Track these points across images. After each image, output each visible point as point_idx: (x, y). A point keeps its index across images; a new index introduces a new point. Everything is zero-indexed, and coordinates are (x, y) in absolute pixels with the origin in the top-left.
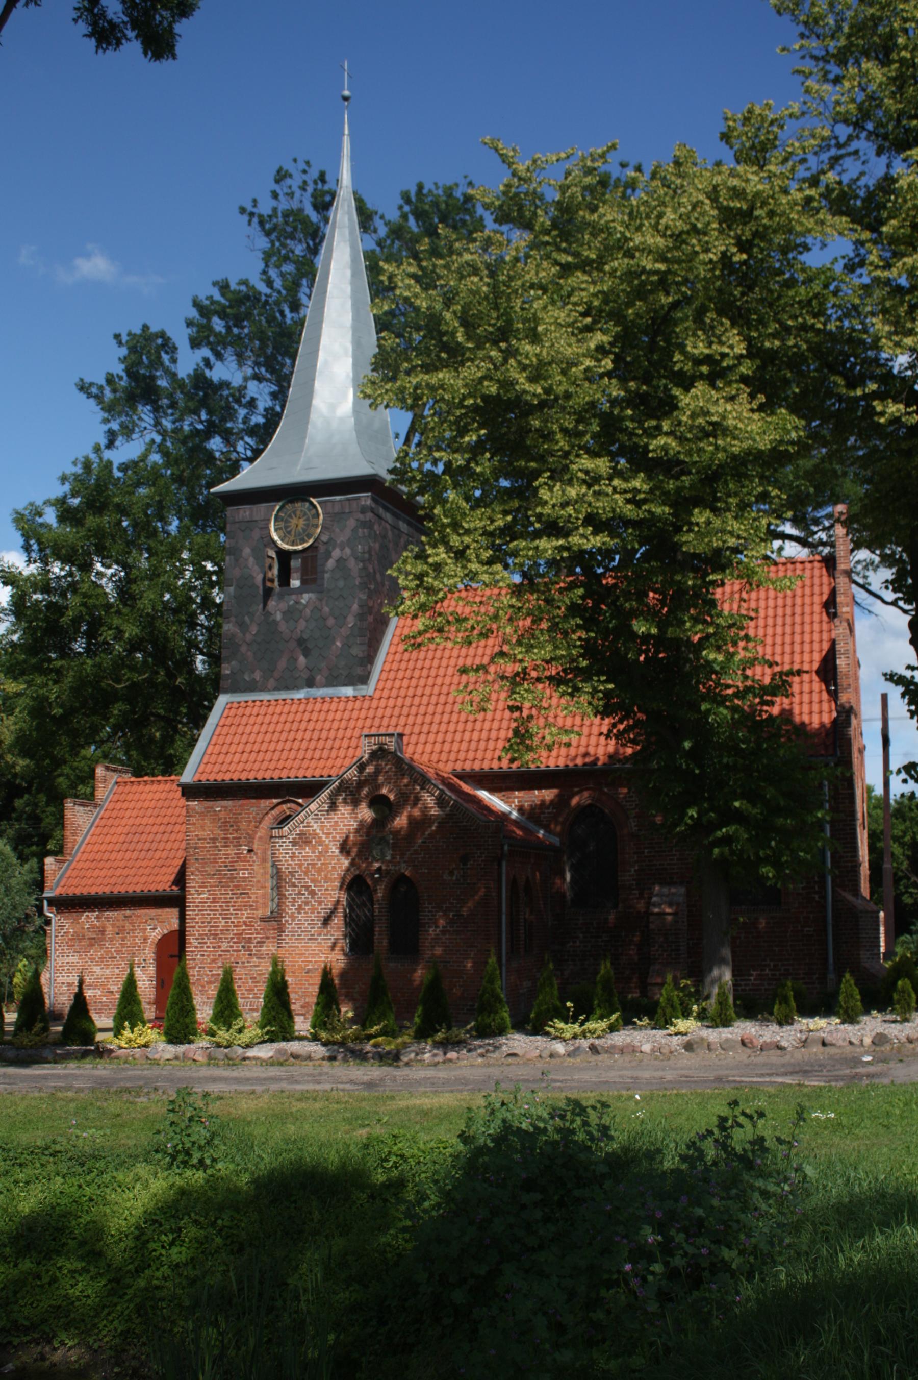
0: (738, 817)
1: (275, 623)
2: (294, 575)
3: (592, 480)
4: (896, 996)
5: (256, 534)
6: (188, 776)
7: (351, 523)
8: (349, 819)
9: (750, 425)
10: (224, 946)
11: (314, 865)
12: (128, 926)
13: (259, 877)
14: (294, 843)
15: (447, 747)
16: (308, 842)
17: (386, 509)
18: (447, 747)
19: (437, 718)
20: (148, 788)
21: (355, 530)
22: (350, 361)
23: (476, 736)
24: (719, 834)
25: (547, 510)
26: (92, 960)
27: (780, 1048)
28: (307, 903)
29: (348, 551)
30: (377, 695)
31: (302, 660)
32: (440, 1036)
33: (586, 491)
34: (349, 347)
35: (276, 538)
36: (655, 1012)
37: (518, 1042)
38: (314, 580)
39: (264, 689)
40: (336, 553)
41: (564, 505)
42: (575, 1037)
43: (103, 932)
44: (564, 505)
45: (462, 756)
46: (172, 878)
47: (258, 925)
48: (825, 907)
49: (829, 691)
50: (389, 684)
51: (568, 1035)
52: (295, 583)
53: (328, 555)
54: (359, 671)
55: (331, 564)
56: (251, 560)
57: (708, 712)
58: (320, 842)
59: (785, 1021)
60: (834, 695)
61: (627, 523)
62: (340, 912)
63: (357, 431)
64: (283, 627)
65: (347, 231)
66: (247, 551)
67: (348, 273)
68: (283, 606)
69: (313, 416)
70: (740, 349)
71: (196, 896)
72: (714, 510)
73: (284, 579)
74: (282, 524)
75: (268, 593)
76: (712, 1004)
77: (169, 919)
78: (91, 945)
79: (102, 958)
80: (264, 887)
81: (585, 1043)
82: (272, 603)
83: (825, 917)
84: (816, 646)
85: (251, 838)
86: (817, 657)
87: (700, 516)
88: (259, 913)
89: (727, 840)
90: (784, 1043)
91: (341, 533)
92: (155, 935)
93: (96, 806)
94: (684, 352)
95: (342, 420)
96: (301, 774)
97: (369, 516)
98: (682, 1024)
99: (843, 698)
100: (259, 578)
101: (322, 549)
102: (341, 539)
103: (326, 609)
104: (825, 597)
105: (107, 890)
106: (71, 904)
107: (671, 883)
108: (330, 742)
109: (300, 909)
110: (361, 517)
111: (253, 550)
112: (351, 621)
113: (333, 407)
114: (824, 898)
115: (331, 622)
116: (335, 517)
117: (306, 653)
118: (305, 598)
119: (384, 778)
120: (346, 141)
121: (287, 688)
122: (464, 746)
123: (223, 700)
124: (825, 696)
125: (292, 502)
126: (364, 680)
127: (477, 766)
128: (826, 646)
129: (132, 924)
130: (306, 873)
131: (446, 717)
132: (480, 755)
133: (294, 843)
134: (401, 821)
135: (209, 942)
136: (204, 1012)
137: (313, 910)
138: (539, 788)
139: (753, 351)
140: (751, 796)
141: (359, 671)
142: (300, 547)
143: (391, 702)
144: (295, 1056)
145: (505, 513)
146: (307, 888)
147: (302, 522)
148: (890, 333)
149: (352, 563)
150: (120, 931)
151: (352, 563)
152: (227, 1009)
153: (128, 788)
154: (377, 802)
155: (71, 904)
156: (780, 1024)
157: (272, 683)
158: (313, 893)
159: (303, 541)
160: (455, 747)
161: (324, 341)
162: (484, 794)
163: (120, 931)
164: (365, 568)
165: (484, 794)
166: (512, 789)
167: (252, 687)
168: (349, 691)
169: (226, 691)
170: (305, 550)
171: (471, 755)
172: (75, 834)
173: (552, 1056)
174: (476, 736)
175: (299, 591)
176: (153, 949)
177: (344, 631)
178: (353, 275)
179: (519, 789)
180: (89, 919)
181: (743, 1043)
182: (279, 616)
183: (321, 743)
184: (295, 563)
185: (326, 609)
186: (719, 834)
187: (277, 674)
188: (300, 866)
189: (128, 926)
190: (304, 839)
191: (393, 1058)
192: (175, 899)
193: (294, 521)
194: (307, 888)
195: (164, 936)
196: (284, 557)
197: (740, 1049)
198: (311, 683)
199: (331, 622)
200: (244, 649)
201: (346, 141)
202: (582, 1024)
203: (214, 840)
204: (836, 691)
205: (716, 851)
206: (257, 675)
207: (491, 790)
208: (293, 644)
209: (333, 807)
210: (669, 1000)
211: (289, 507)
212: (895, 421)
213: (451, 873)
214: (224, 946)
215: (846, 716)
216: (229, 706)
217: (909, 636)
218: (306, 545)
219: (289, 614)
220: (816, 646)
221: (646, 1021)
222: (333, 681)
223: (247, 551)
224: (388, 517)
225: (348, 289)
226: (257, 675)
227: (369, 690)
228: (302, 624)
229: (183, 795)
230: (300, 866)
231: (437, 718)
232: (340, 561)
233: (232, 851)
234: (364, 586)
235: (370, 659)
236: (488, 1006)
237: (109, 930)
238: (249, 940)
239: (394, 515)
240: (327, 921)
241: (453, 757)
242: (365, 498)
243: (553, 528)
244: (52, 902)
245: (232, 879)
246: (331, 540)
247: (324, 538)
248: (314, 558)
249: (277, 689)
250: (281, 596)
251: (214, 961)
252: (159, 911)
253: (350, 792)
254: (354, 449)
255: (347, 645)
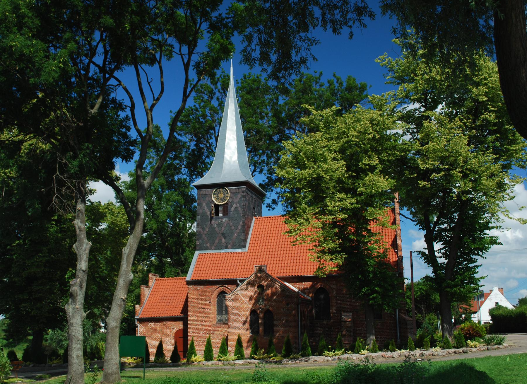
0: (376, 292)
1: (214, 228)
2: (220, 212)
3: (340, 200)
4: (424, 343)
5: (207, 199)
6: (189, 278)
7: (239, 196)
8: (252, 291)
9: (384, 183)
10: (201, 333)
11: (239, 307)
12: (165, 328)
13: (213, 311)
14: (233, 300)
15: (274, 269)
16: (237, 299)
17: (249, 191)
18: (274, 269)
19: (270, 259)
20: (167, 281)
21: (240, 198)
22: (236, 142)
23: (283, 265)
24: (371, 297)
25: (330, 208)
26: (152, 339)
27: (393, 357)
28: (237, 319)
29: (238, 205)
30: (249, 252)
31: (223, 240)
32: (291, 356)
33: (340, 203)
34: (236, 138)
35: (214, 200)
36: (354, 349)
37: (313, 358)
38: (227, 214)
39: (211, 249)
40: (234, 206)
41: (334, 207)
42: (332, 356)
43: (156, 330)
44: (334, 207)
45: (279, 271)
46: (180, 311)
47: (213, 326)
48: (396, 319)
49: (395, 251)
50: (253, 248)
51: (330, 355)
52: (221, 215)
53: (232, 206)
54: (243, 244)
55: (233, 209)
56: (206, 207)
57: (368, 261)
58: (241, 299)
59: (393, 351)
60: (397, 253)
61: (349, 209)
62: (248, 321)
63: (239, 165)
64: (217, 229)
65: (233, 99)
66: (204, 204)
67: (234, 113)
68: (217, 222)
69: (225, 161)
70: (377, 162)
71: (192, 317)
72: (374, 207)
73: (217, 213)
74: (216, 196)
75: (212, 218)
76: (371, 346)
77: (180, 325)
78: (152, 334)
79: (156, 338)
80: (214, 314)
81: (337, 357)
82: (213, 221)
83: (396, 322)
84: (390, 237)
85: (210, 298)
86: (391, 240)
87: (370, 209)
88: (213, 323)
89: (374, 298)
90: (394, 356)
91: (237, 201)
92: (174, 330)
93: (150, 287)
94: (362, 162)
95: (234, 162)
96: (216, 278)
97: (245, 194)
98: (363, 352)
99: (400, 254)
100: (209, 213)
101: (230, 204)
102: (236, 201)
103: (231, 224)
104: (392, 221)
105: (158, 316)
106: (144, 320)
107: (347, 312)
108: (235, 267)
109: (235, 320)
110: (243, 194)
111: (206, 204)
112: (240, 228)
113: (231, 157)
114: (396, 316)
115: (233, 228)
116: (234, 194)
117: (225, 238)
118: (224, 220)
119: (261, 280)
120: (232, 69)
121: (218, 249)
122: (280, 268)
123: (197, 253)
124: (394, 253)
125: (219, 188)
126: (244, 247)
127: (284, 275)
128: (393, 237)
129: (166, 327)
130: (237, 309)
131: (272, 259)
132: (285, 271)
133: (233, 300)
134: (269, 292)
135: (196, 332)
136: (216, 351)
137: (239, 321)
138: (305, 282)
139: (381, 161)
140: (379, 286)
141: (243, 244)
142: (222, 203)
143: (254, 254)
144: (250, 363)
145: (318, 208)
146: (237, 314)
147: (222, 195)
148: (422, 164)
149: (240, 209)
150: (162, 329)
151: (240, 209)
152: (224, 350)
153: (159, 282)
154: (260, 287)
155: (144, 320)
156: (391, 351)
157: (213, 247)
158: (239, 315)
159: (223, 201)
160: (277, 268)
161: (227, 135)
162: (287, 284)
163: (162, 329)
164: (244, 210)
165: (287, 284)
166: (296, 282)
167: (207, 249)
168: (239, 250)
169: (198, 250)
170: (224, 204)
171: (282, 271)
172: (144, 297)
173: (327, 361)
174: (283, 265)
175: (222, 218)
176: (174, 335)
177: (238, 231)
178: (236, 113)
179: (298, 282)
180: (151, 325)
181: (382, 356)
182: (215, 226)
183: (232, 267)
184: (221, 209)
185: (231, 224)
186: (371, 297)
187: (215, 245)
188: (235, 307)
189: (165, 328)
190: (236, 299)
191: (280, 362)
192: (184, 318)
193: (220, 195)
194: (237, 314)
195: (177, 331)
196: (217, 206)
197: (382, 358)
198: (226, 248)
199: (233, 228)
200: (204, 236)
201: (232, 69)
202: (334, 352)
203: (197, 299)
204: (397, 252)
205: (371, 302)
206: (208, 245)
207: (289, 283)
208: (220, 235)
209: (247, 288)
210: (359, 345)
211: (218, 190)
212: (424, 186)
213: (283, 309)
214: (201, 333)
215: (401, 258)
216: (200, 255)
217: (424, 239)
218: (224, 203)
219: (219, 225)
220: (390, 237)
221: (350, 352)
222: (234, 247)
223: (204, 204)
224: (250, 193)
225: (234, 118)
226: (208, 245)
227: (246, 250)
228: (223, 228)
229: (187, 284)
230: (235, 307)
231: (270, 259)
232: (236, 208)
233: (203, 302)
234: (244, 216)
235: (245, 240)
236: (304, 348)
237: (158, 329)
238: (210, 331)
239: (251, 193)
240: (244, 324)
241: (276, 272)
242: (244, 188)
243: (331, 213)
244: (138, 320)
245: (204, 311)
246: (232, 201)
247: (230, 201)
248: (227, 207)
249: (215, 249)
250: (216, 219)
251: (198, 338)
252: (175, 322)
253: (251, 284)
254: (239, 171)
255: (238, 235)
